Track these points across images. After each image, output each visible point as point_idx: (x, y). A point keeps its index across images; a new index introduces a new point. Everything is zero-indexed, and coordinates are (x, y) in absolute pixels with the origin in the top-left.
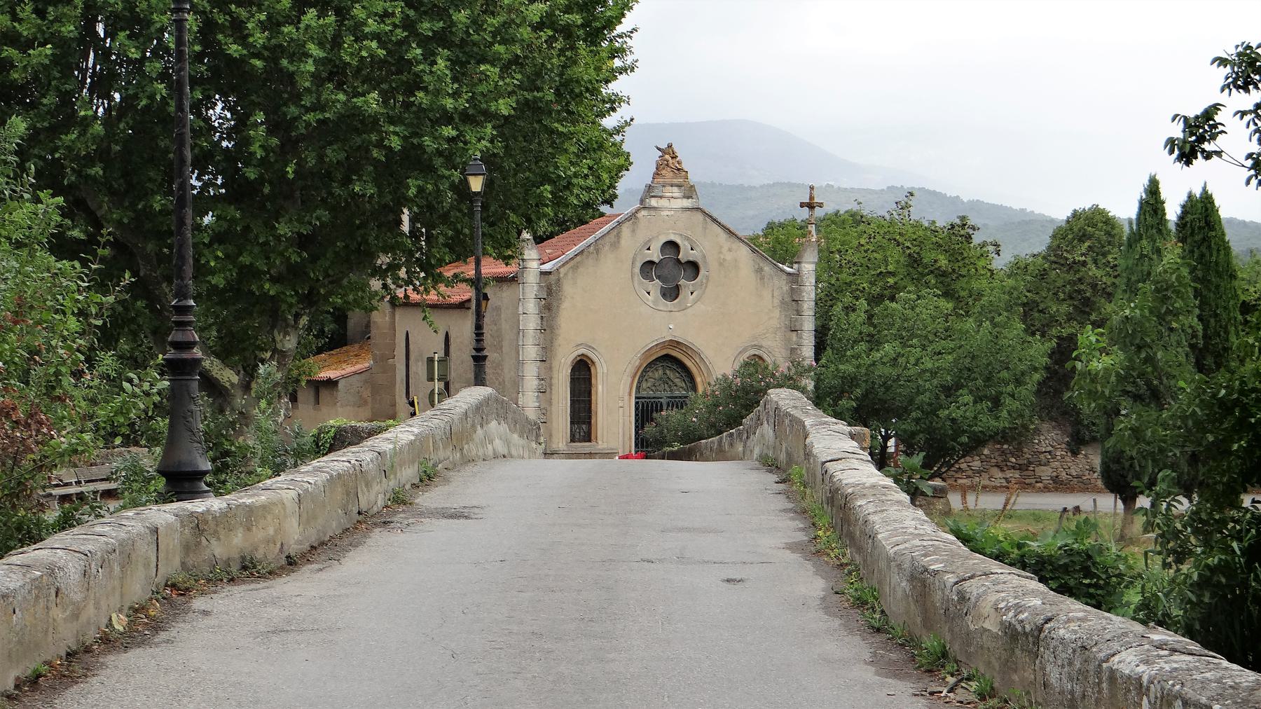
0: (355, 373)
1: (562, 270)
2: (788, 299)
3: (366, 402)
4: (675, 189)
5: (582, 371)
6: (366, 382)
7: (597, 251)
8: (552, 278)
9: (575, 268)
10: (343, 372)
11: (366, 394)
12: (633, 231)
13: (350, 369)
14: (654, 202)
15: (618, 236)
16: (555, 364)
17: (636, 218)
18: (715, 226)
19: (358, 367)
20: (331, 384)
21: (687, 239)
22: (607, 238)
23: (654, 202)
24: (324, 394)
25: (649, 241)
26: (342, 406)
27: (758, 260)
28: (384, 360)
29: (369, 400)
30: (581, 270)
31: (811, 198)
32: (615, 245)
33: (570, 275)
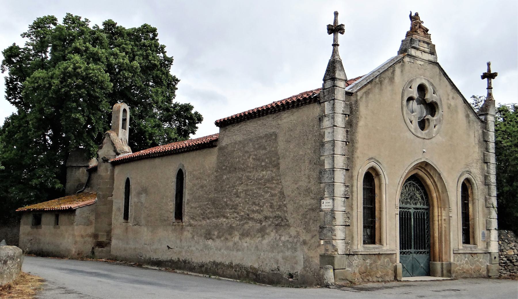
0: (87, 205)
1: (359, 93)
2: (482, 140)
3: (91, 223)
4: (426, 45)
5: (371, 178)
6: (92, 211)
7: (381, 82)
8: (353, 98)
9: (367, 93)
10: (79, 205)
11: (92, 218)
12: (402, 71)
13: (81, 203)
14: (413, 52)
15: (393, 72)
16: (355, 174)
17: (404, 62)
18: (445, 79)
19: (87, 202)
20: (71, 211)
21: (432, 85)
22: (387, 73)
23: (413, 52)
24: (63, 218)
25: (411, 81)
26: (77, 225)
27: (467, 109)
28: (106, 198)
29: (94, 221)
30: (371, 96)
31: (489, 70)
32: (392, 79)
33: (364, 99)
